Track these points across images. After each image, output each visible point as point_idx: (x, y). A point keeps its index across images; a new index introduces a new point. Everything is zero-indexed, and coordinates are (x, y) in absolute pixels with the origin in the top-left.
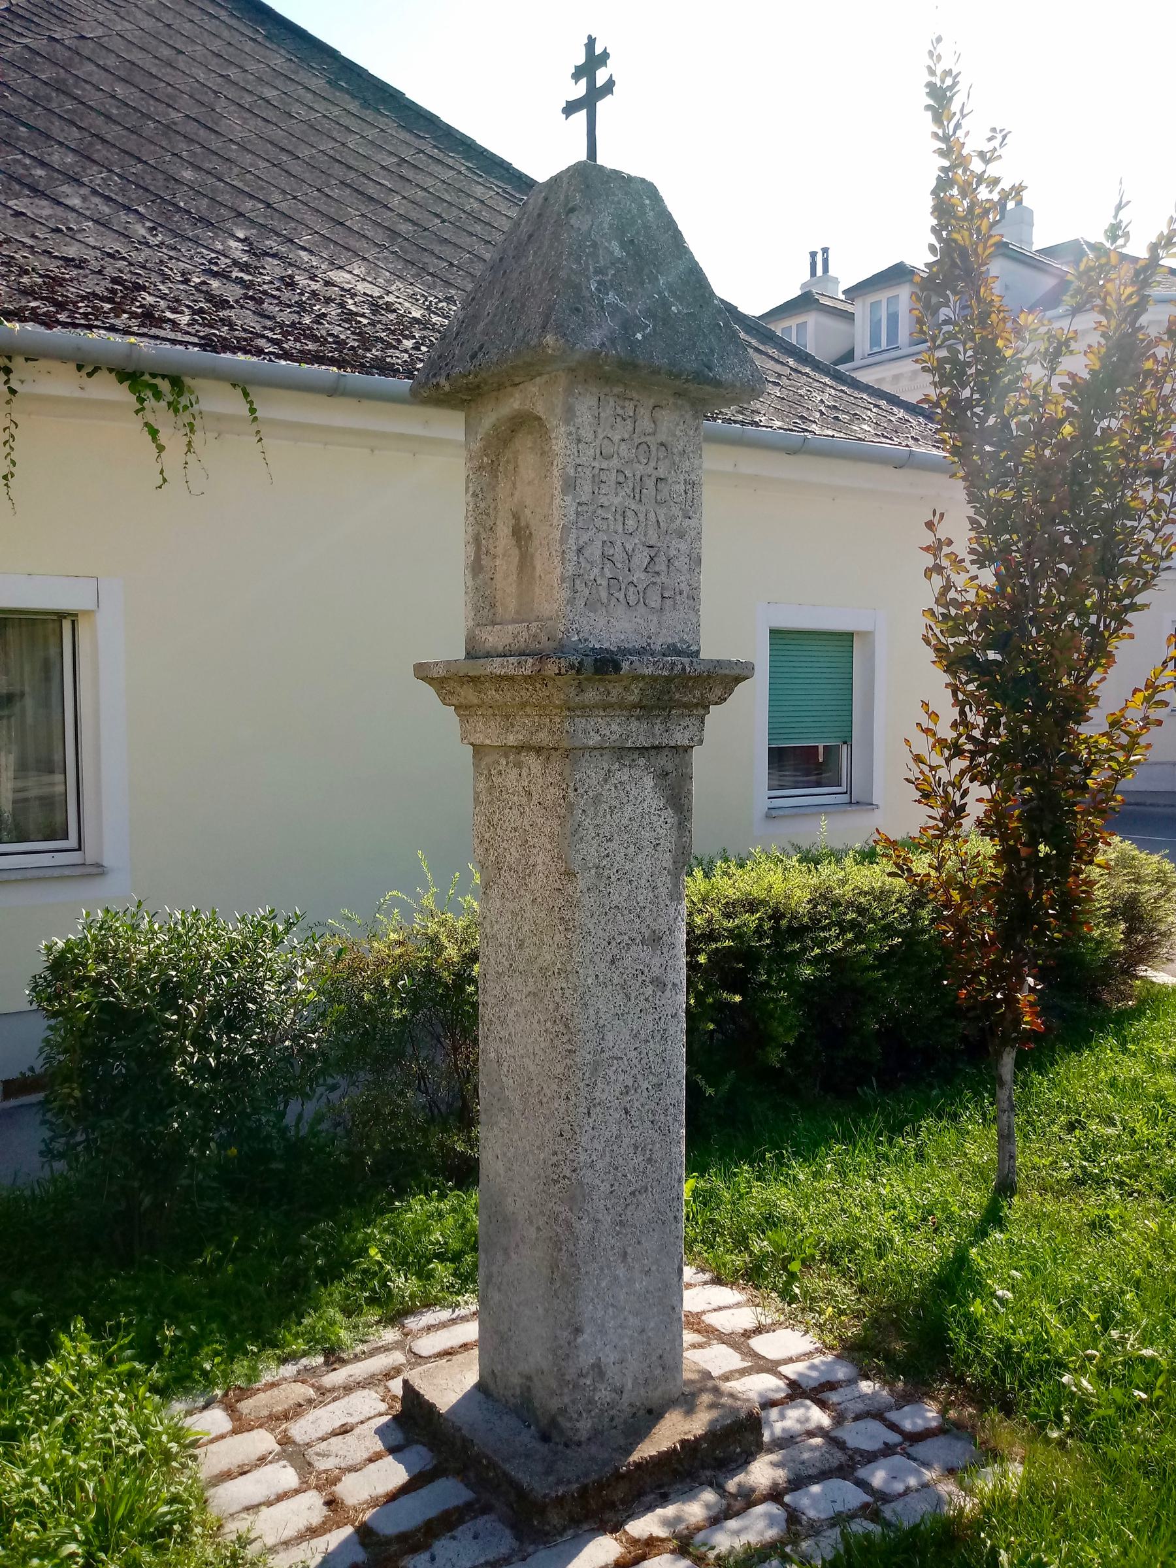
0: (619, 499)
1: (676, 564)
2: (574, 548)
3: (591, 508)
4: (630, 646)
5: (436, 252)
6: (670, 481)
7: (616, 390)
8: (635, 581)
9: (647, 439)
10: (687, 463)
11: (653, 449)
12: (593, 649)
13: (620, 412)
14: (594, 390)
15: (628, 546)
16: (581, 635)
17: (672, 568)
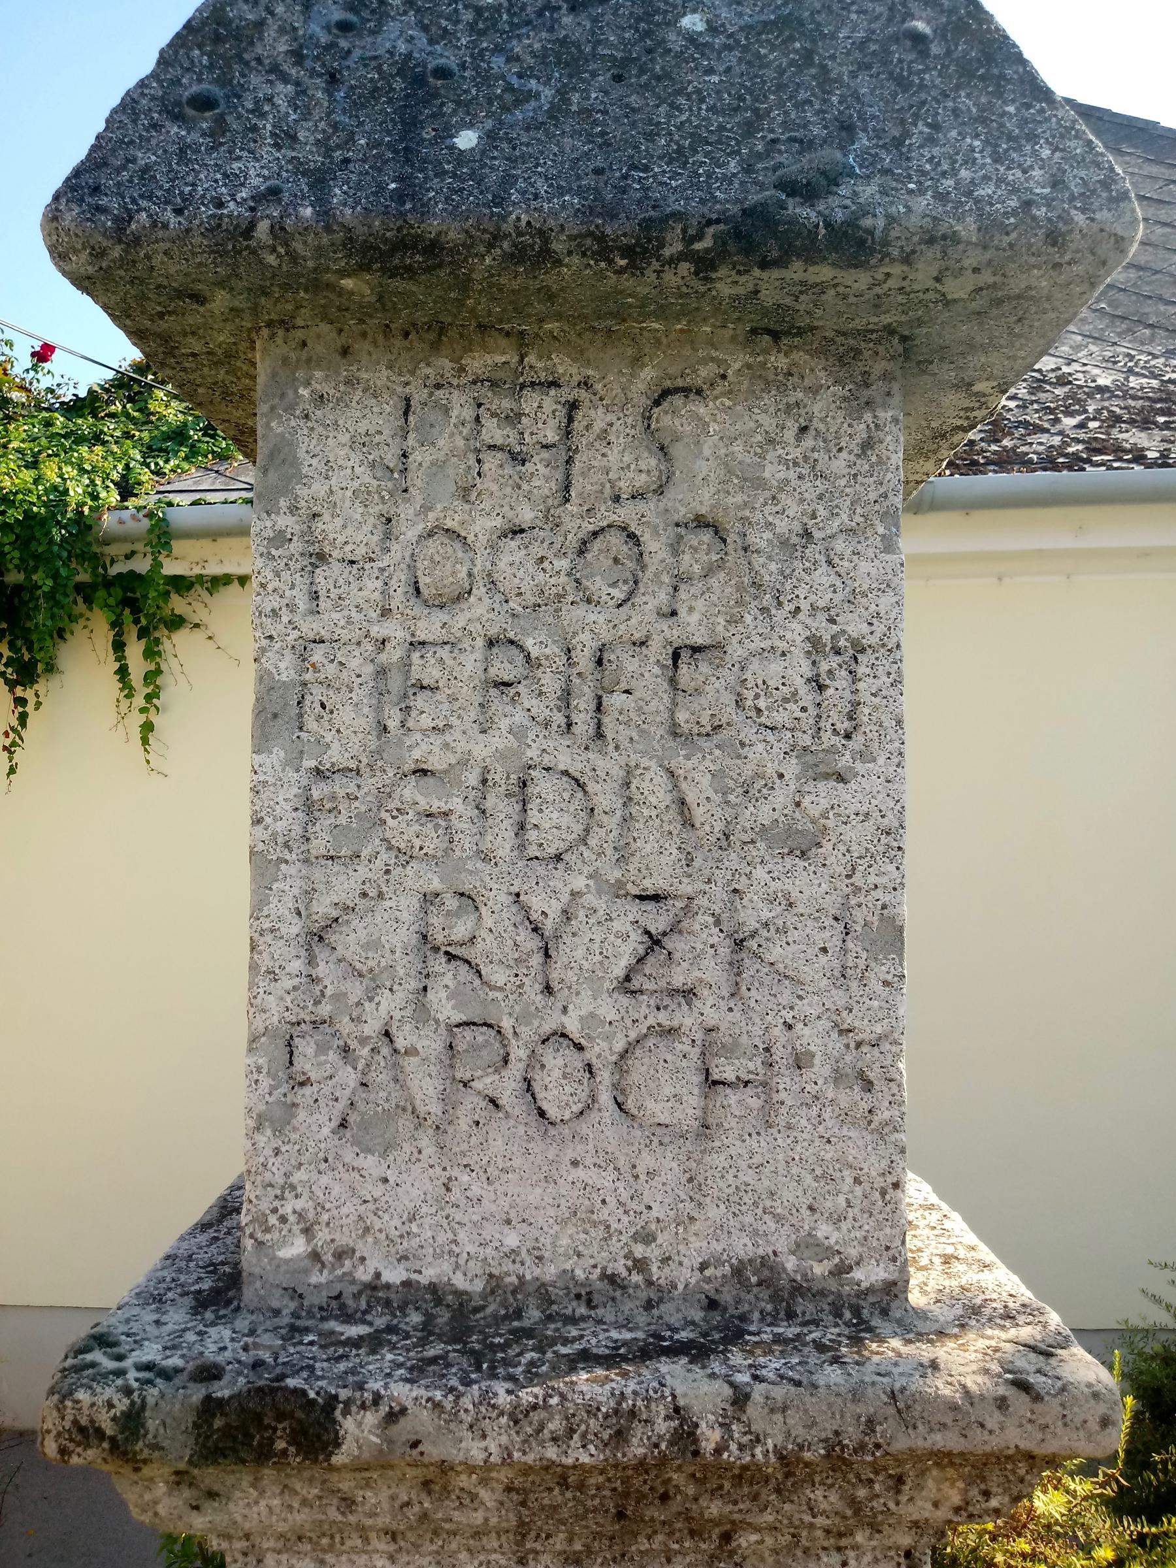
0: (499, 740)
1: (775, 952)
2: (294, 928)
3: (370, 783)
4: (549, 1272)
5: (1167, 296)
6: (736, 652)
7: (477, 363)
8: (572, 1026)
9: (626, 513)
10: (823, 576)
11: (655, 547)
12: (374, 1286)
13: (493, 431)
14: (381, 376)
15: (537, 902)
16: (322, 1236)
17: (751, 967)
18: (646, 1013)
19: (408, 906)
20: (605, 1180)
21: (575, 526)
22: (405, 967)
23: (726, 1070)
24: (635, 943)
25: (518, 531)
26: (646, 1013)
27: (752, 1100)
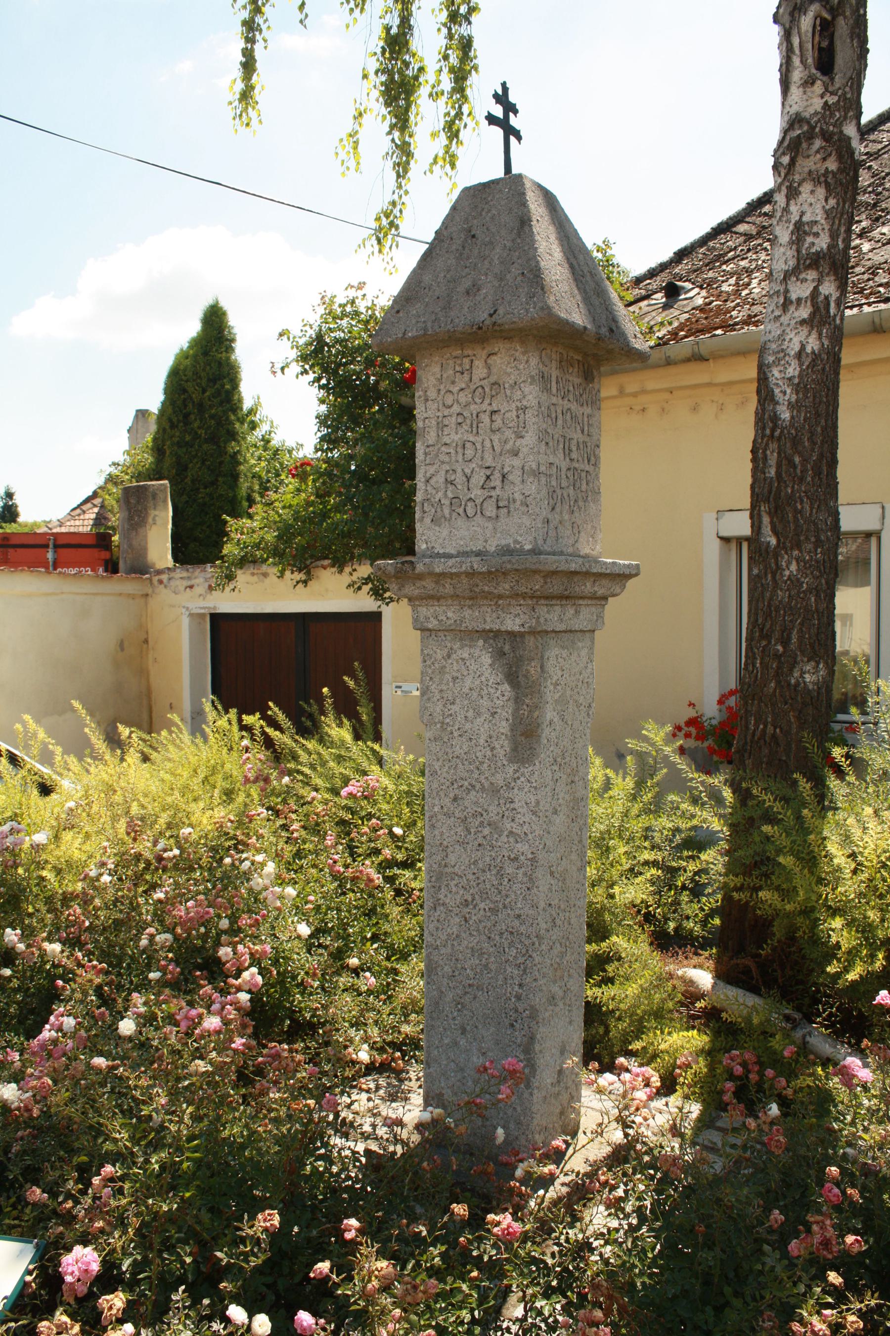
7: (455, 353)
9: (482, 383)
11: (487, 390)
13: (458, 368)
18: (486, 493)
19: (443, 473)
20: (478, 529)
21: (473, 387)
22: (443, 486)
23: (501, 504)
24: (484, 478)
25: (462, 389)
26: (486, 493)
27: (505, 510)
